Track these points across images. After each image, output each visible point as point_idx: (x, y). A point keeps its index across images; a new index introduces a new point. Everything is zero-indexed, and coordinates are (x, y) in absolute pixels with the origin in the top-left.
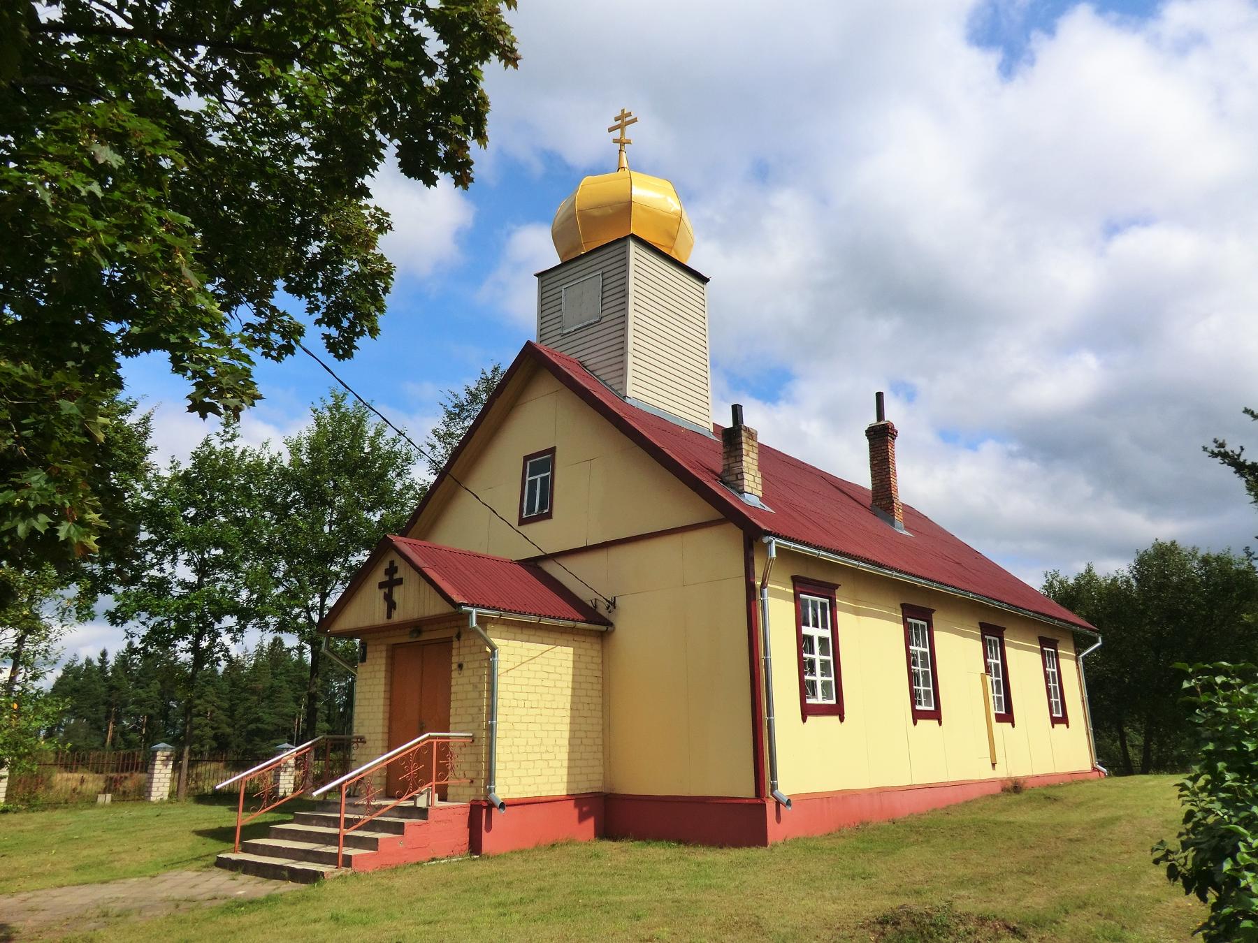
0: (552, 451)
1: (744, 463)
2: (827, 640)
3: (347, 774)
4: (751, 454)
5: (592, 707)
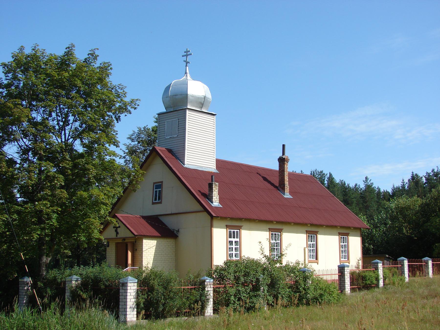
0: (162, 182)
1: (213, 194)
2: (238, 241)
3: (409, 271)
4: (216, 191)
5: (172, 259)
